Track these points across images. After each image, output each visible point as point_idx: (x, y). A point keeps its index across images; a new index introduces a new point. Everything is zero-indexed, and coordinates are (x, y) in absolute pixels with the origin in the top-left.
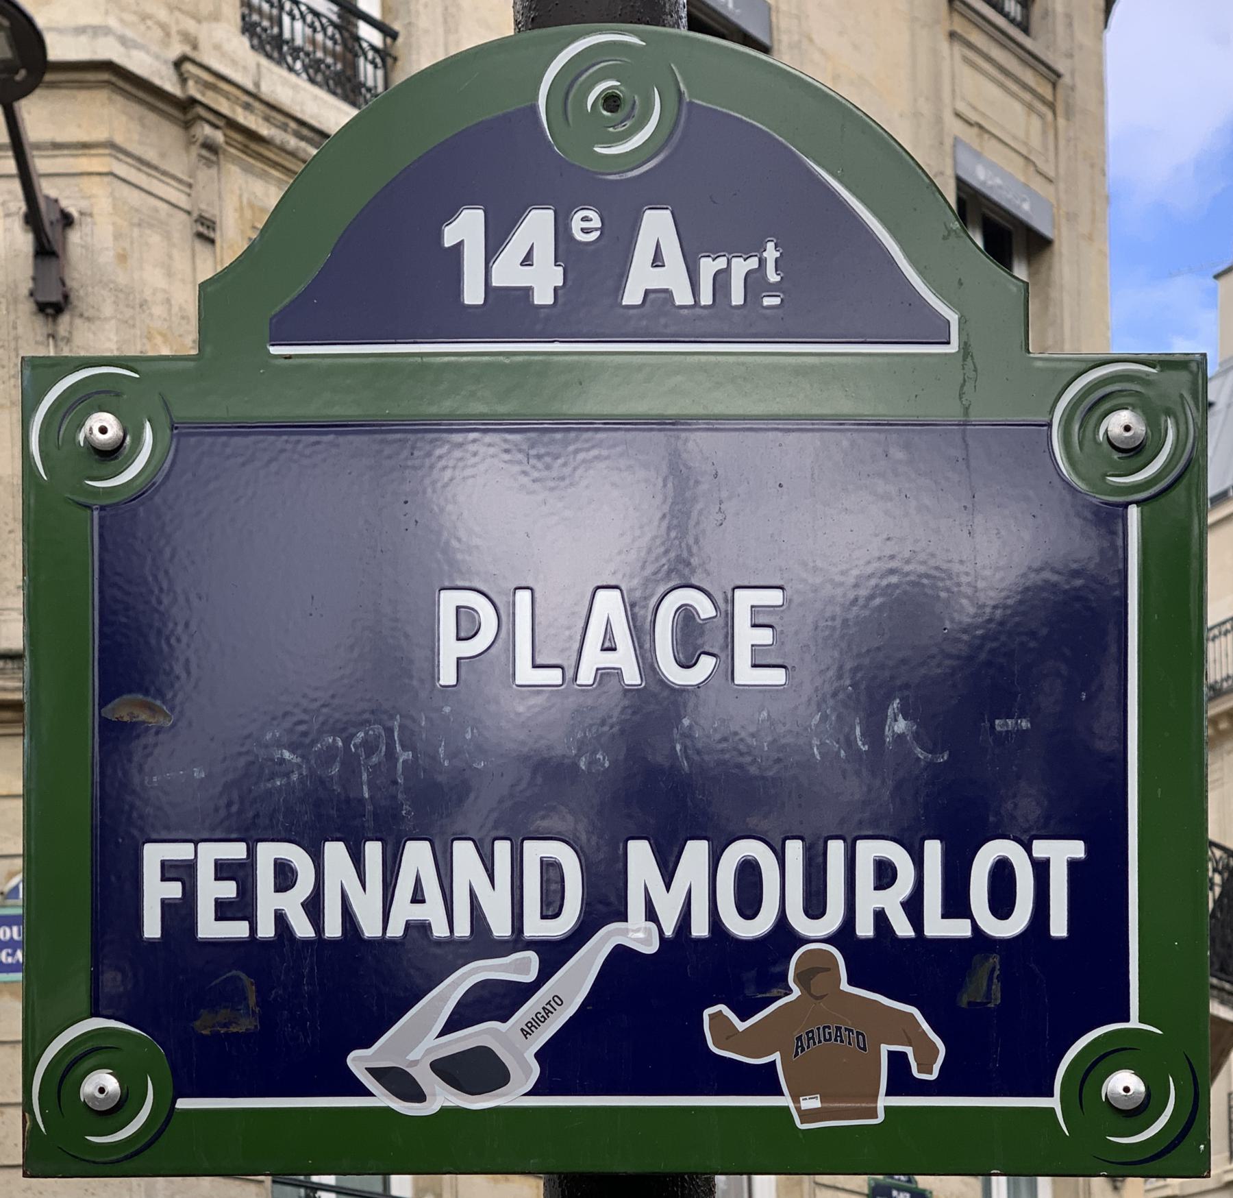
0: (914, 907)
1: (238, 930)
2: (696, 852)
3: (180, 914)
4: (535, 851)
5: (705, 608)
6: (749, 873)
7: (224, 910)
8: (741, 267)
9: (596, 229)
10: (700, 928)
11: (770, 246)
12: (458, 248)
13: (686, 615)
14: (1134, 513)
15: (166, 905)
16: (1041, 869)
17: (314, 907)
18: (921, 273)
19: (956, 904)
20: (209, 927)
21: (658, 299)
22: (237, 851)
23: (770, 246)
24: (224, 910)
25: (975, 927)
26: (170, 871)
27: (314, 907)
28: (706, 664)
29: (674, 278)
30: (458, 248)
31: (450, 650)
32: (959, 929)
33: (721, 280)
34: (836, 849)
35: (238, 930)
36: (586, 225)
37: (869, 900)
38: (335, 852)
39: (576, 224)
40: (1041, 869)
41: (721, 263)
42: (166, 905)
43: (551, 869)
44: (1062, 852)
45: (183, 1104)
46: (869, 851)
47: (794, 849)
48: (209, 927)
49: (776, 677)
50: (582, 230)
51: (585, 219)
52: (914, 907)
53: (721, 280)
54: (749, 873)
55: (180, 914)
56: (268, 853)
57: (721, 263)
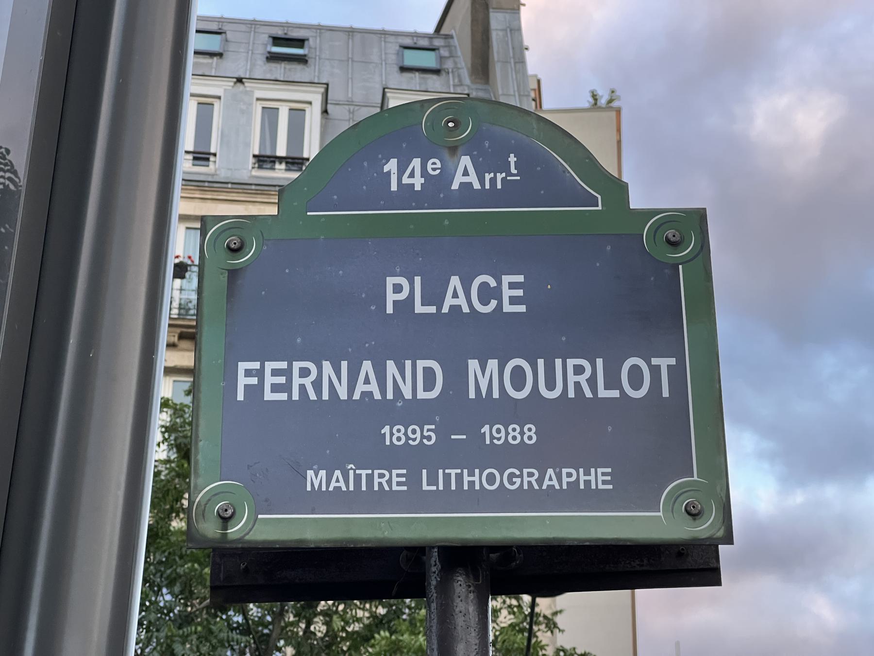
0: (592, 382)
1: (283, 396)
3: (254, 392)
4: (421, 364)
5: (493, 283)
6: (518, 373)
7: (275, 388)
8: (500, 176)
10: (496, 395)
11: (512, 155)
12: (389, 173)
13: (484, 286)
15: (247, 387)
16: (655, 371)
17: (317, 385)
19: (613, 382)
20: (269, 396)
21: (466, 187)
23: (512, 155)
25: (622, 392)
26: (248, 373)
27: (317, 385)
28: (494, 303)
29: (473, 178)
30: (389, 173)
31: (391, 297)
33: (493, 181)
34: (558, 362)
35: (283, 396)
37: (572, 378)
38: (327, 366)
39: (429, 166)
40: (655, 371)
41: (492, 175)
42: (247, 387)
44: (664, 363)
46: (571, 362)
47: (541, 362)
49: (522, 308)
52: (592, 382)
53: (493, 181)
54: (518, 373)
56: (297, 365)
57: (492, 175)
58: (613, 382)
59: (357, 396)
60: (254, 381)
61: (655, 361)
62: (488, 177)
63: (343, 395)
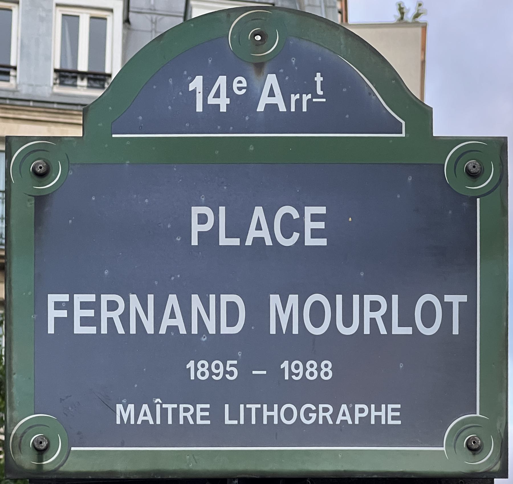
0: (387, 318)
1: (92, 330)
2: (293, 299)
3: (64, 325)
4: (225, 298)
5: (296, 215)
6: (317, 307)
7: (85, 321)
8: (306, 98)
9: (244, 88)
14: (478, 200)
16: (447, 307)
17: (125, 318)
18: (454, 425)
19: (406, 319)
20: (78, 329)
22: (91, 298)
24: (85, 321)
26: (58, 306)
27: (125, 318)
28: (296, 236)
29: (278, 100)
32: (408, 331)
33: (299, 102)
35: (92, 330)
36: (240, 83)
38: (134, 299)
39: (235, 85)
43: (232, 307)
45: (73, 449)
46: (368, 298)
48: (78, 329)
50: (238, 88)
51: (240, 82)
52: (387, 318)
53: (299, 102)
55: (64, 325)
56: (105, 298)
58: (406, 319)
59: (163, 331)
60: (63, 314)
61: (447, 298)
62: (294, 98)
63: (150, 329)
